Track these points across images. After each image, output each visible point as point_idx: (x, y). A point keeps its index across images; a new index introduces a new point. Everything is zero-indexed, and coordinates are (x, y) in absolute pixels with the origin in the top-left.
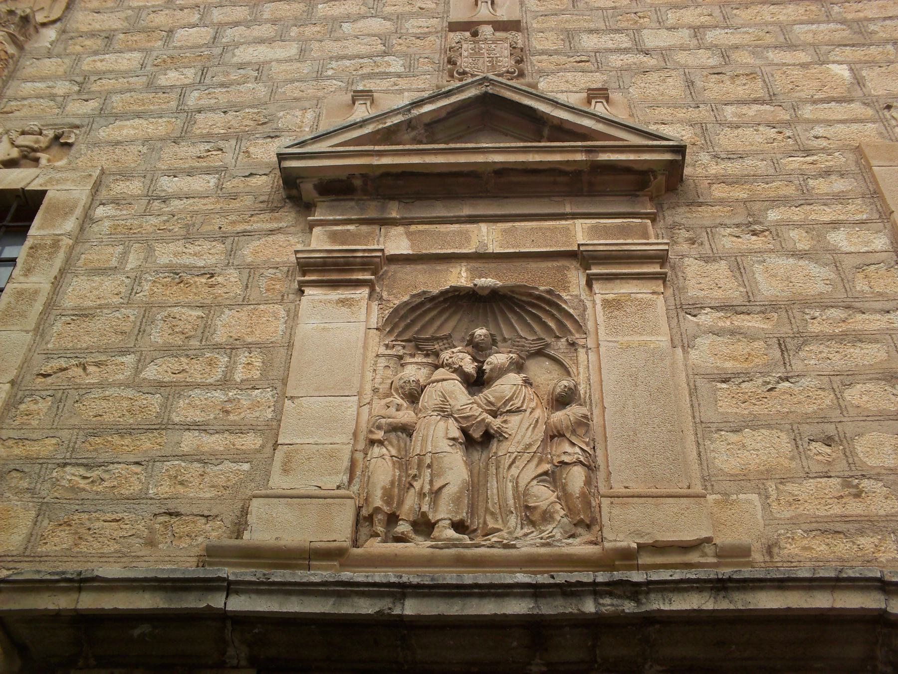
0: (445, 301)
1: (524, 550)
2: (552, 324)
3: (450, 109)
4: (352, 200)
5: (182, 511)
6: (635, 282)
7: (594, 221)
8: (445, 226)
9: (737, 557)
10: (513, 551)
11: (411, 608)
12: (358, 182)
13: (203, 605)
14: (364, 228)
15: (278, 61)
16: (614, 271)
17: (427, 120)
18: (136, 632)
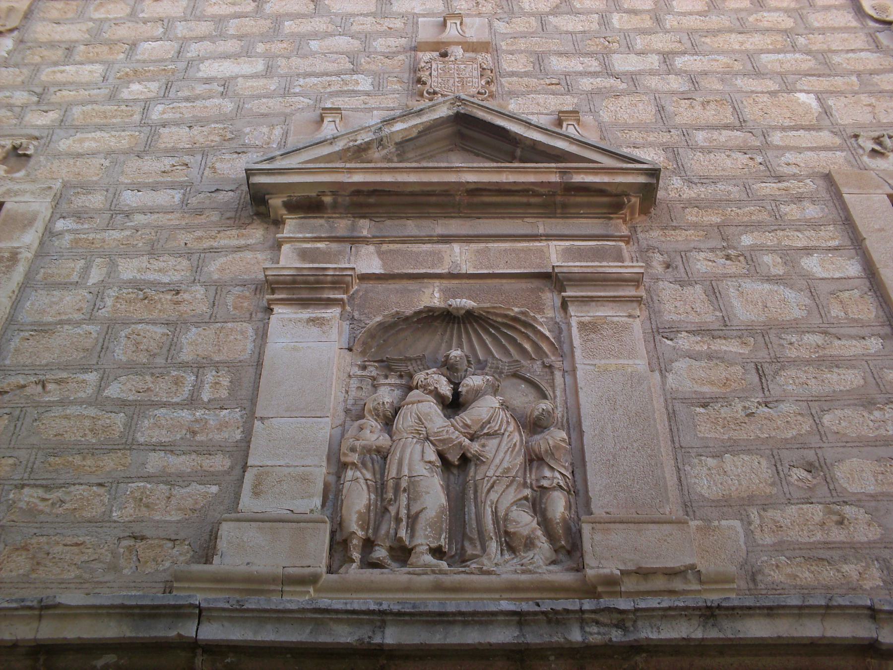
0: (419, 321)
1: (503, 576)
2: (527, 346)
3: (421, 128)
4: (323, 217)
5: (147, 533)
6: (611, 304)
7: (568, 243)
8: (417, 245)
9: (716, 582)
10: (493, 578)
11: (391, 636)
12: (328, 199)
13: (172, 634)
14: (334, 246)
15: (245, 77)
16: (589, 294)
17: (398, 139)
18: (100, 663)
